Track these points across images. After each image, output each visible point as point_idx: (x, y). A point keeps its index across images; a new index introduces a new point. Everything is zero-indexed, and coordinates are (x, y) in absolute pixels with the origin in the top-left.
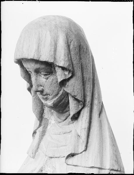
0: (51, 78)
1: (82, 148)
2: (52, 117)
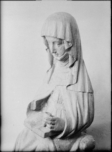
0: (61, 46)
2: (58, 64)
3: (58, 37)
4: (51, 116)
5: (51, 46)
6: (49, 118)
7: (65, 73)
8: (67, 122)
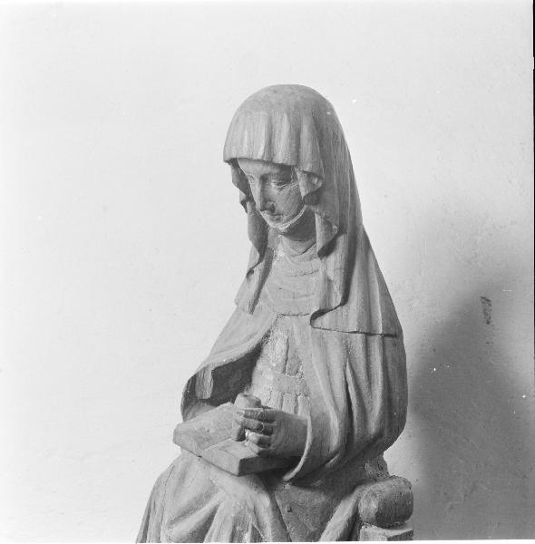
0: (287, 189)
1: (337, 298)
2: (283, 249)
3: (275, 161)
4: (258, 404)
5: (256, 189)
6: (252, 411)
7: (303, 274)
8: (313, 425)
